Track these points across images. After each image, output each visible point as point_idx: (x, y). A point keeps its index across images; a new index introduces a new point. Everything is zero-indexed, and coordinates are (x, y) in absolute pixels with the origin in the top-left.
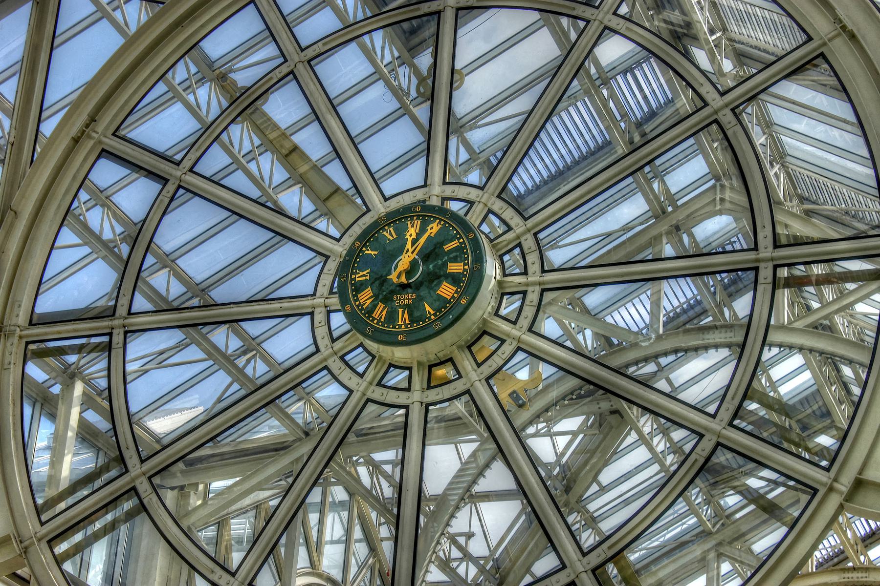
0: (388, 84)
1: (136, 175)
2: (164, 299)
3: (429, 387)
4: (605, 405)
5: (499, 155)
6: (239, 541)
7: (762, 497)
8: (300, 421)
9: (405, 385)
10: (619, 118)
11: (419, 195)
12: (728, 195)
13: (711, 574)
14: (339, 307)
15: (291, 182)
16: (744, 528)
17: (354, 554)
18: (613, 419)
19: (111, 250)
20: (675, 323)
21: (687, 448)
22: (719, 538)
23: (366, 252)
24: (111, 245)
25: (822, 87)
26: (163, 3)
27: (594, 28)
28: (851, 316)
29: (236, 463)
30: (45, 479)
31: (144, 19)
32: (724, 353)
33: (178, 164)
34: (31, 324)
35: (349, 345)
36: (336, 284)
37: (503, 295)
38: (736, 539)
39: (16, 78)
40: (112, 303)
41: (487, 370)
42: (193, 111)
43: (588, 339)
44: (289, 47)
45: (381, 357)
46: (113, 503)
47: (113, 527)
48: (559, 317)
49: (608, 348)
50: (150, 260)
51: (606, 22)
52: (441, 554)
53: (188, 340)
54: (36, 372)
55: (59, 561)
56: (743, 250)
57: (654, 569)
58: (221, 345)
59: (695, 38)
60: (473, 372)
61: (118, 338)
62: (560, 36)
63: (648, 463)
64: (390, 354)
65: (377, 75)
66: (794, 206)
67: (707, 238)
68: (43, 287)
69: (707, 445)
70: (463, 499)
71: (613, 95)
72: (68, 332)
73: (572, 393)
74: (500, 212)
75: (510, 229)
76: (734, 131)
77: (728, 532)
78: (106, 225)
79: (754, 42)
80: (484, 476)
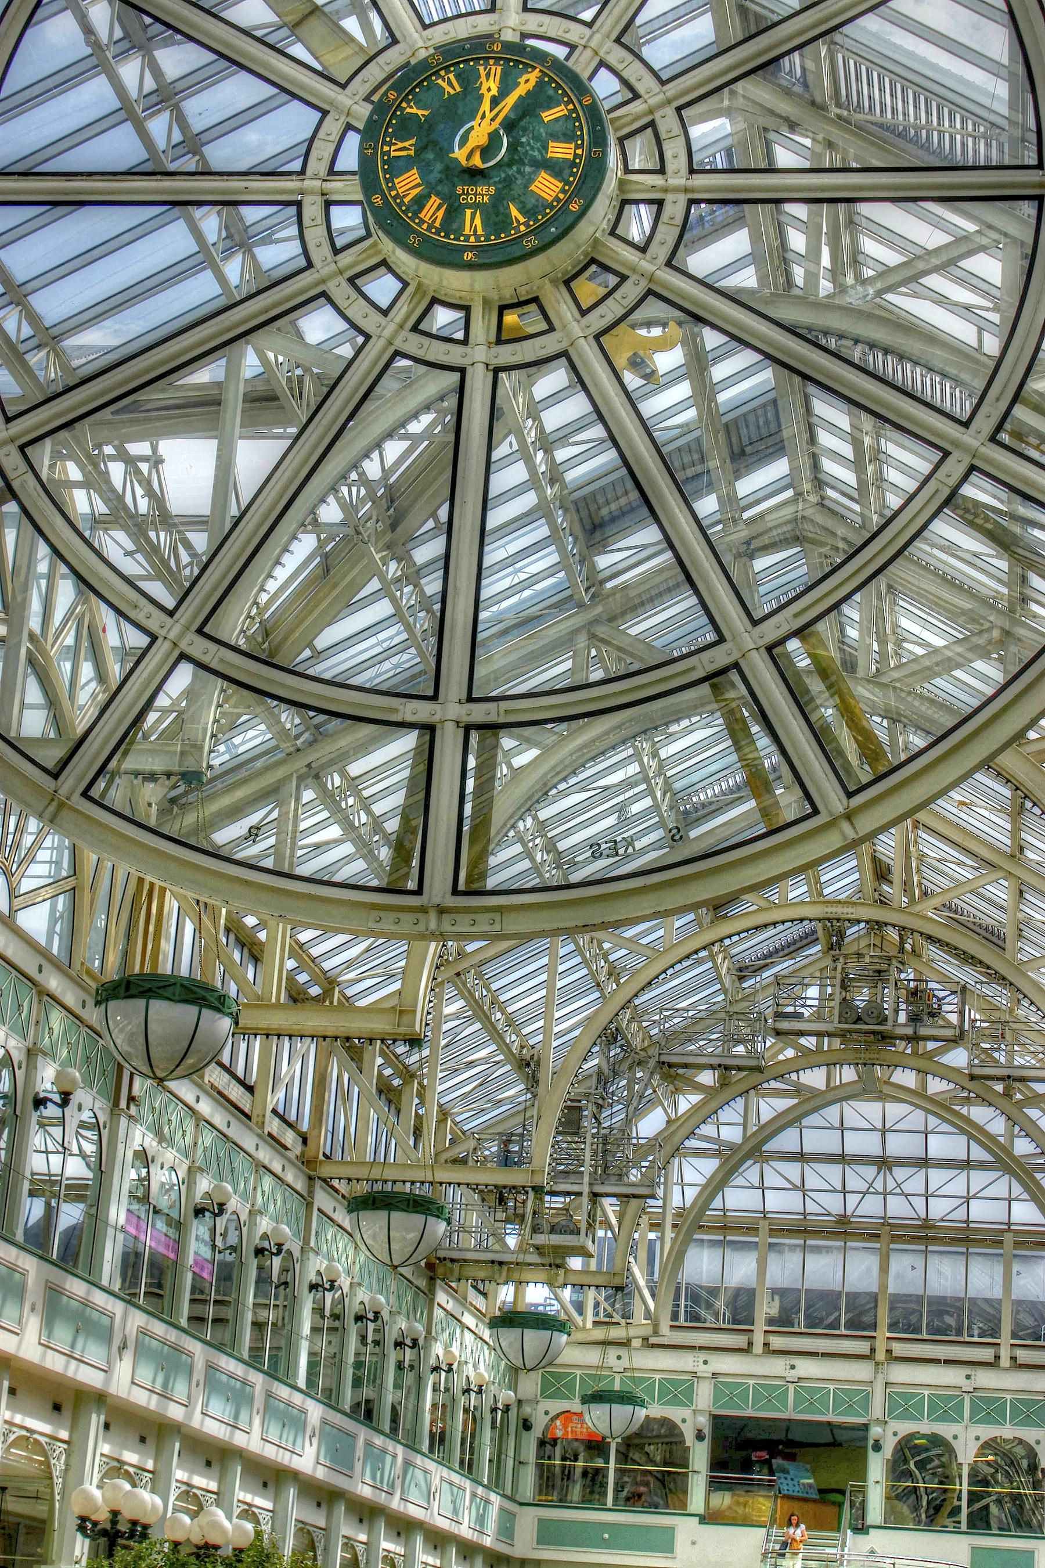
3: (499, 341)
11: (483, 24)
23: (408, 110)
35: (363, 261)
37: (624, 202)
60: (575, 324)
64: (436, 278)
74: (619, 67)
75: (636, 96)
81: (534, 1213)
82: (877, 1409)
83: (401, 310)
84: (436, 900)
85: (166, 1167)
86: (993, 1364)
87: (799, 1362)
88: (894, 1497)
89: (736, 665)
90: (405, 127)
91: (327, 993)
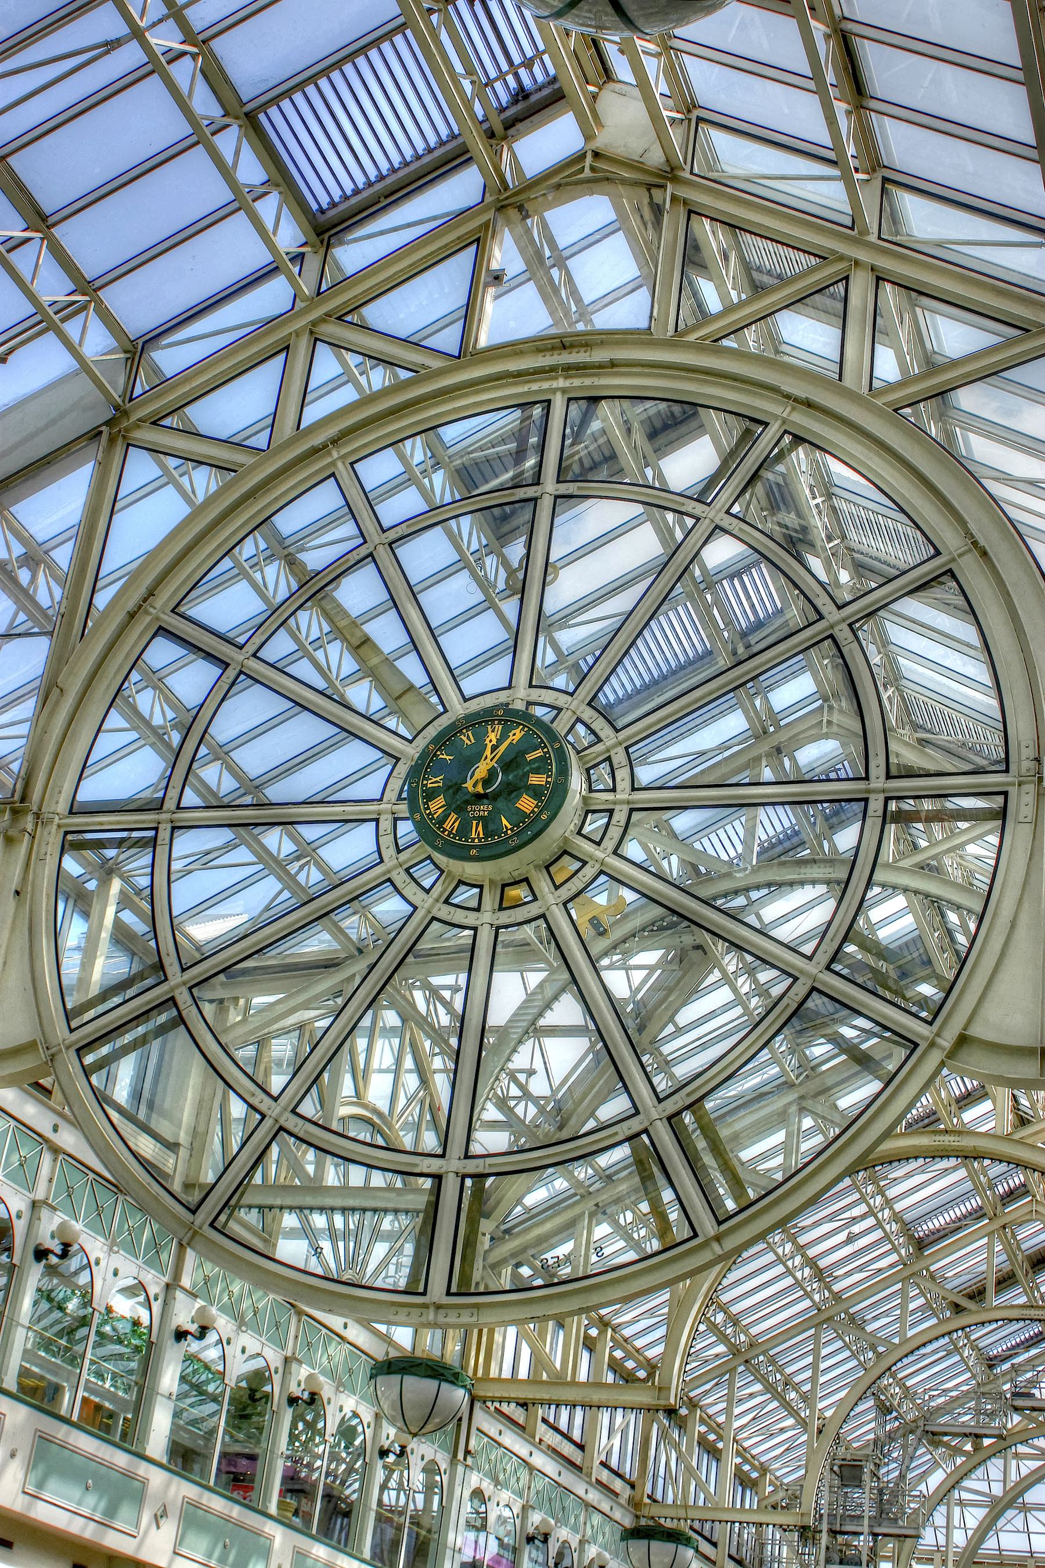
0: (474, 575)
1: (194, 657)
2: (215, 795)
3: (501, 908)
4: (688, 940)
5: (590, 660)
6: (279, 1063)
7: (856, 1047)
8: (354, 937)
9: (474, 904)
10: (722, 626)
11: (503, 697)
12: (836, 718)
13: (790, 1129)
14: (408, 815)
15: (360, 674)
16: (829, 1082)
17: (403, 1085)
18: (696, 955)
19: (160, 737)
20: (770, 853)
21: (776, 991)
22: (802, 1091)
24: (161, 731)
25: (946, 607)
26: (235, 471)
27: (704, 526)
28: (961, 857)
29: (280, 979)
30: (75, 982)
31: (213, 487)
32: (822, 889)
33: (241, 647)
34: (71, 812)
36: (406, 788)
37: (587, 812)
38: (819, 1093)
39: (71, 543)
40: (160, 794)
41: (565, 893)
42: (260, 591)
43: (673, 866)
44: (370, 527)
45: (449, 873)
46: (143, 1016)
47: (142, 1042)
48: (644, 840)
49: (694, 876)
50: (203, 750)
51: (717, 521)
52: (499, 1093)
53: (237, 840)
54: (72, 866)
55: (87, 1072)
56: (848, 779)
57: (729, 1120)
58: (273, 847)
59: (812, 545)
61: (164, 834)
62: (664, 533)
63: (730, 1005)
64: (461, 870)
65: (462, 564)
66: (906, 732)
67: (810, 763)
68: (86, 773)
69: (801, 989)
70: (527, 1032)
71: (717, 602)
72: (110, 823)
73: (653, 924)
74: (589, 722)
75: (599, 740)
76: (850, 649)
77: (812, 1086)
78: (157, 709)
79: (873, 552)
80: (551, 1009)
81: (827, 1548)
83: (436, 892)
84: (435, 1299)
85: (501, 1504)
89: (646, 1131)
91: (651, 1375)
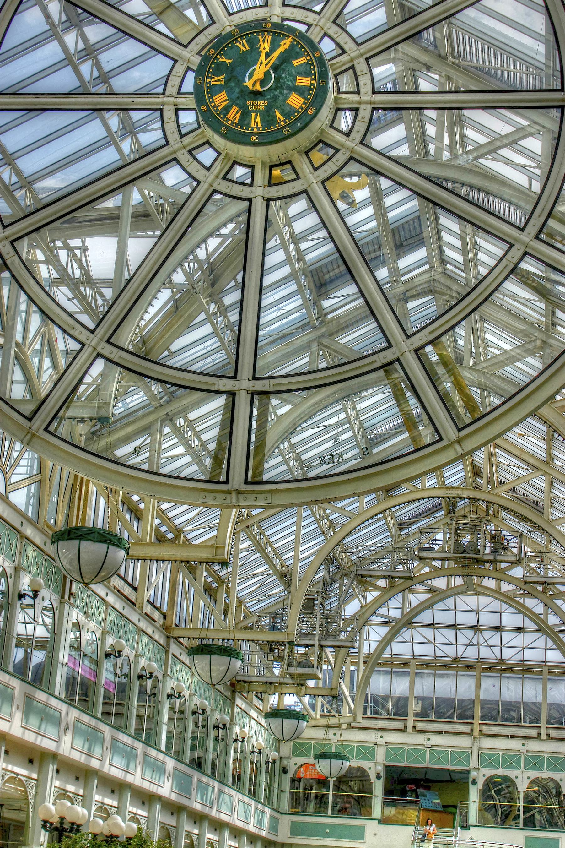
3: (270, 185)
11: (261, 13)
23: (221, 60)
35: (196, 141)
37: (338, 110)
60: (311, 175)
74: (335, 36)
75: (344, 52)
82: (474, 762)
83: (217, 168)
84: (236, 487)
85: (90, 631)
86: (537, 738)
87: (432, 737)
88: (483, 809)
89: (398, 360)
90: (219, 69)
91: (177, 537)
